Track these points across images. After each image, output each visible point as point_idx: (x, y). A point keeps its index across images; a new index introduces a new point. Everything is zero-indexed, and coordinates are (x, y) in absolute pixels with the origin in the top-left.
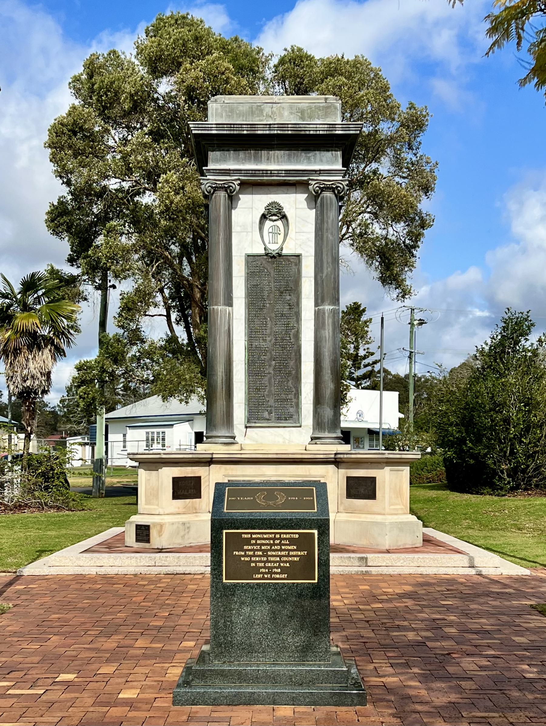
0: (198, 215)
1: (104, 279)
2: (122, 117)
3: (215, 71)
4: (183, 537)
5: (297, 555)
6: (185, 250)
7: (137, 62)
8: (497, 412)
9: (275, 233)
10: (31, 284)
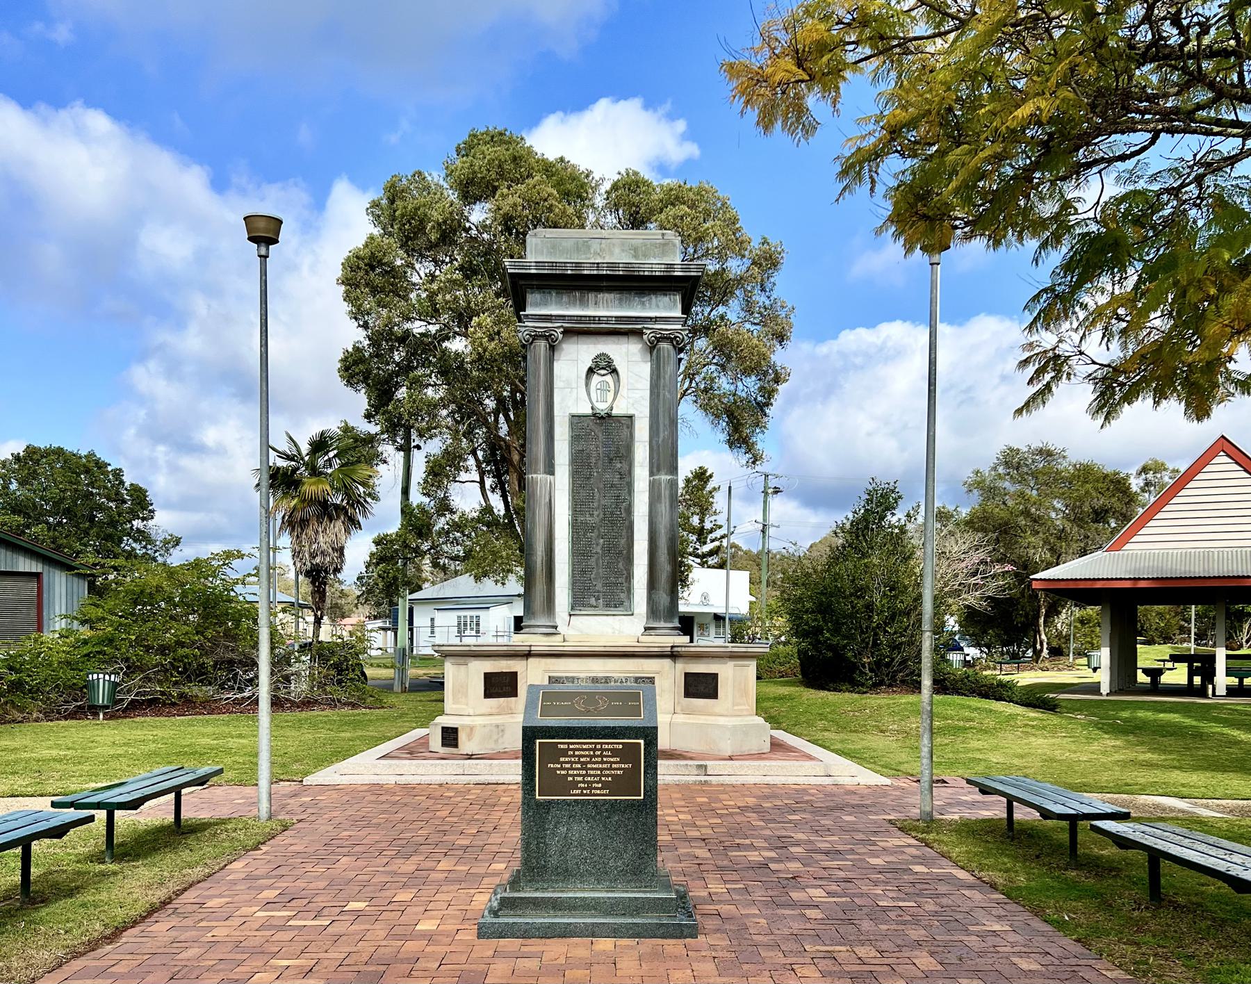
0: (517, 366)
1: (407, 438)
2: (429, 249)
3: (536, 197)
4: (496, 741)
5: (619, 768)
6: (501, 406)
7: (446, 186)
8: (858, 597)
9: (603, 389)
10: (320, 445)
